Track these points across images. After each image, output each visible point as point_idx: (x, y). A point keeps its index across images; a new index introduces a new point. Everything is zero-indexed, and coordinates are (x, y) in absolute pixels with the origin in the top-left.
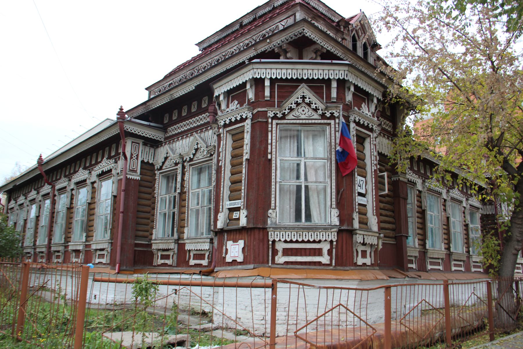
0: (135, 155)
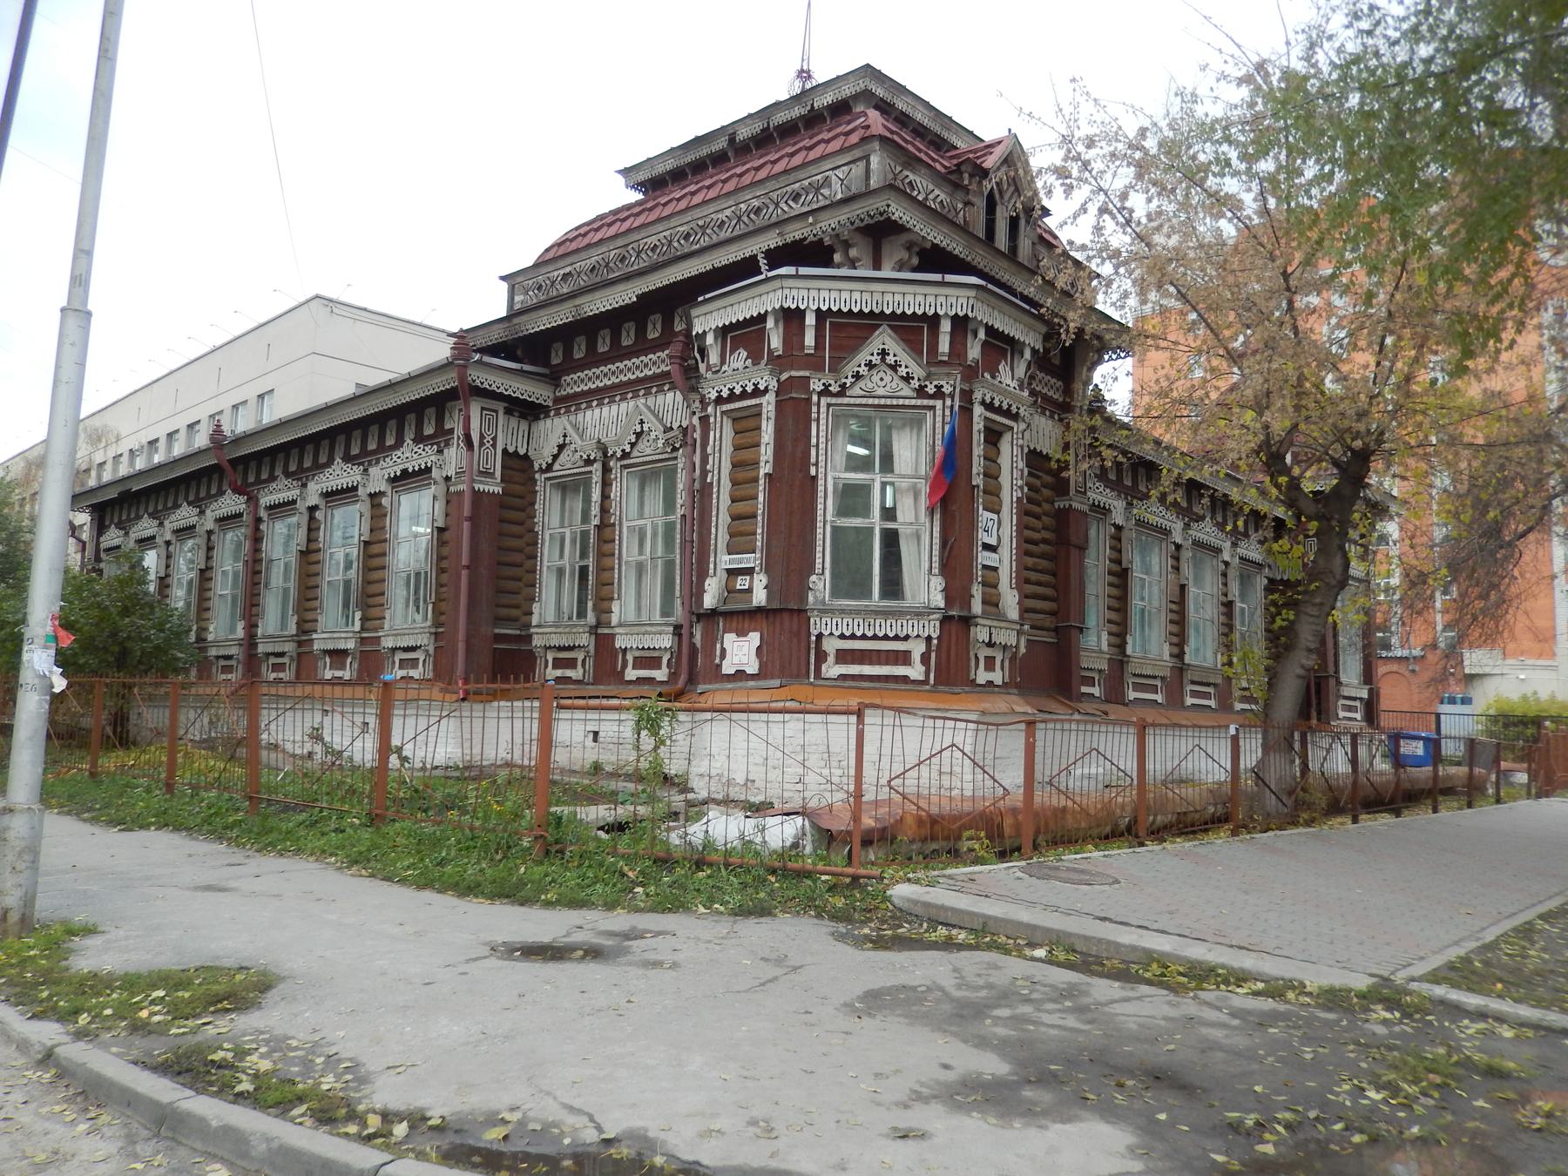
0: (489, 438)
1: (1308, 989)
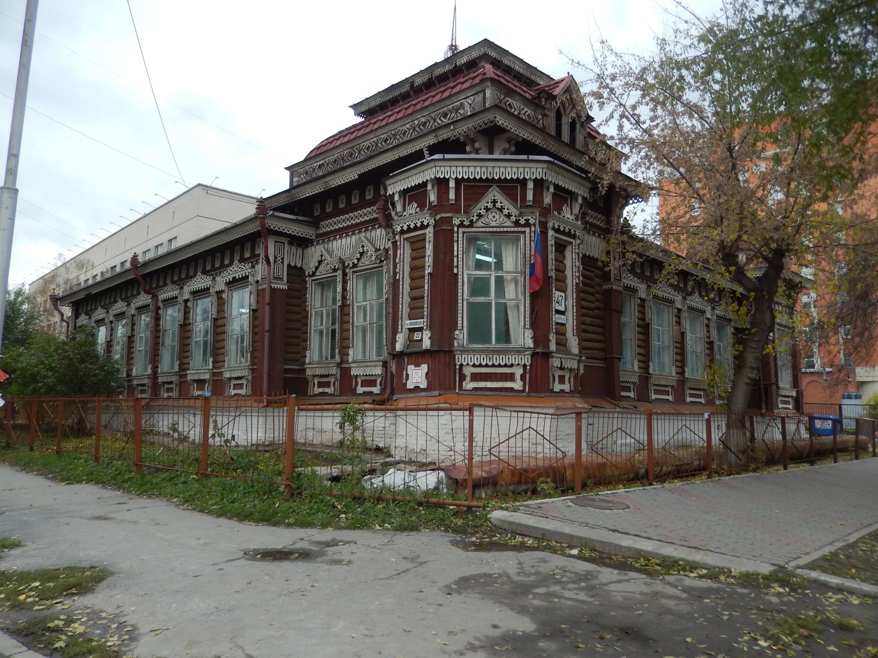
0: (279, 258)
1: (733, 574)
